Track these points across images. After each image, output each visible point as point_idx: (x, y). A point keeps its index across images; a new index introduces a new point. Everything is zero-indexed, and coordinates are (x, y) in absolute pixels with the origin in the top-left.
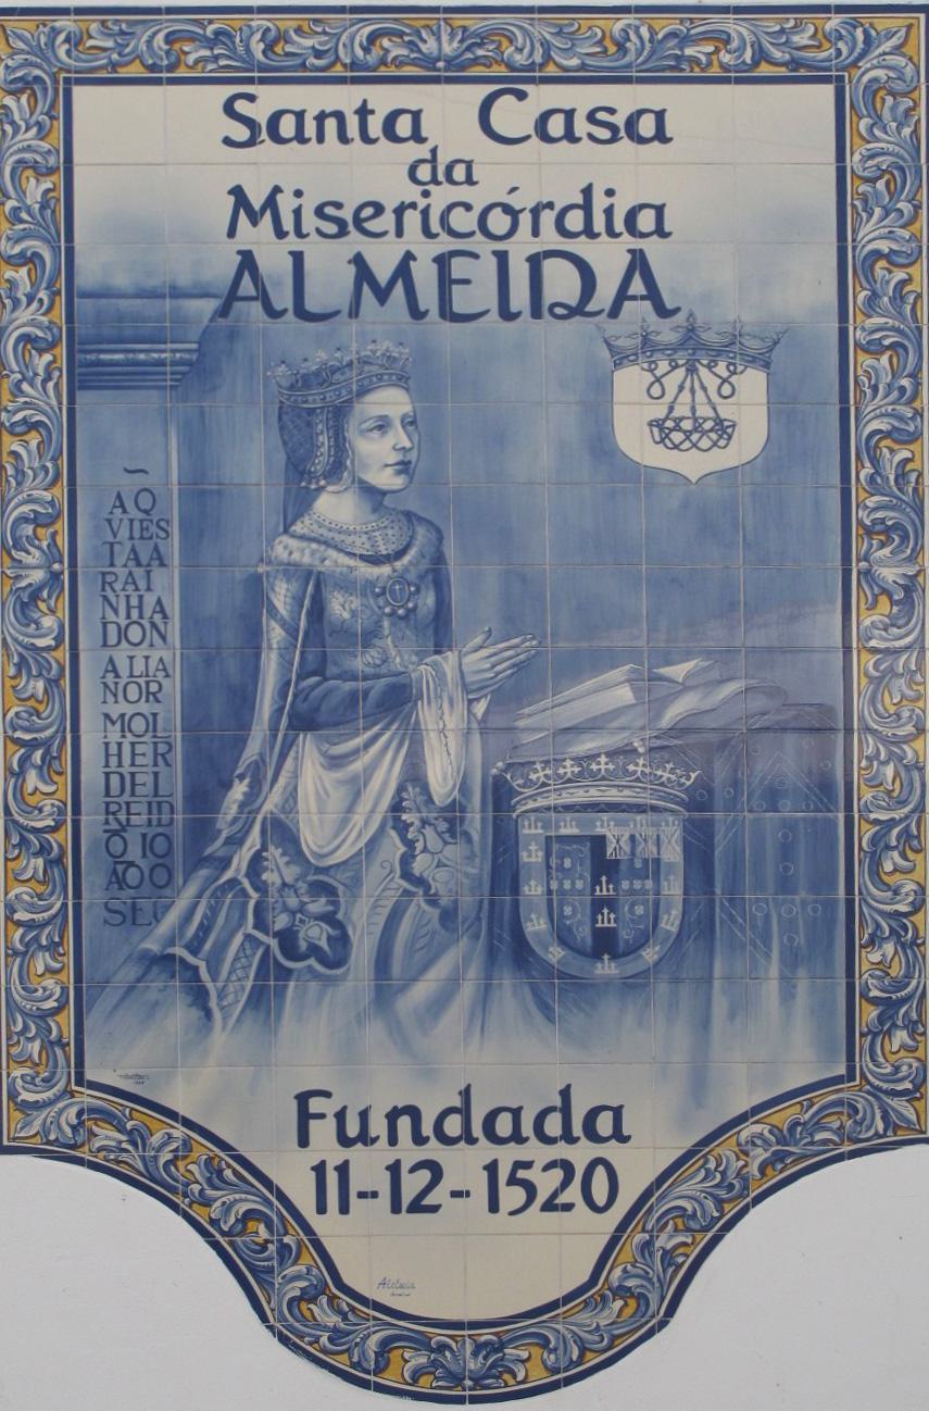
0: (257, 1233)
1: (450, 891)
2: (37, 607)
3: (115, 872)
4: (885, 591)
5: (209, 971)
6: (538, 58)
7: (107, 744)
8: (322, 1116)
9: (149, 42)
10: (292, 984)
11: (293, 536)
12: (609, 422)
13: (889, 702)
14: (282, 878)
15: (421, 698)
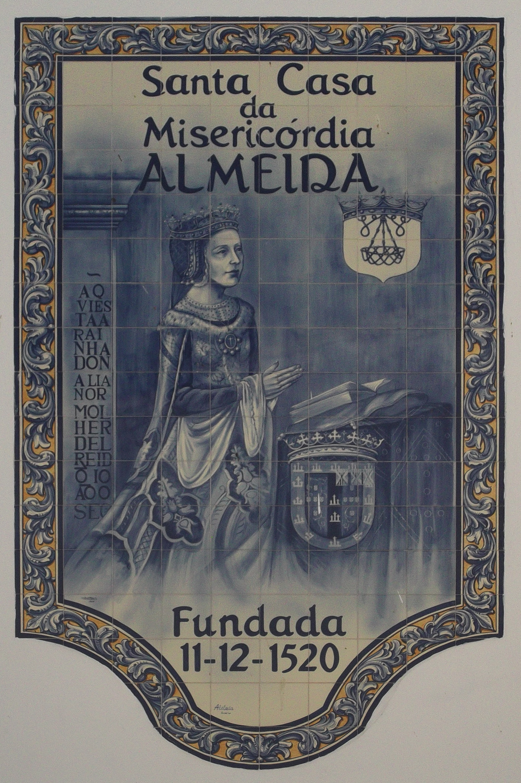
0: (152, 680)
1: (255, 502)
2: (40, 347)
3: (80, 490)
4: (478, 342)
5: (129, 543)
6: (309, 47)
7: (77, 422)
8: (187, 620)
9: (104, 37)
10: (172, 551)
11: (177, 311)
12: (341, 249)
13: (479, 402)
14: (168, 494)
15: (242, 399)
